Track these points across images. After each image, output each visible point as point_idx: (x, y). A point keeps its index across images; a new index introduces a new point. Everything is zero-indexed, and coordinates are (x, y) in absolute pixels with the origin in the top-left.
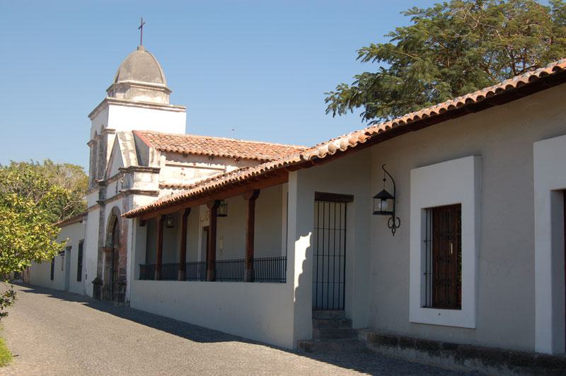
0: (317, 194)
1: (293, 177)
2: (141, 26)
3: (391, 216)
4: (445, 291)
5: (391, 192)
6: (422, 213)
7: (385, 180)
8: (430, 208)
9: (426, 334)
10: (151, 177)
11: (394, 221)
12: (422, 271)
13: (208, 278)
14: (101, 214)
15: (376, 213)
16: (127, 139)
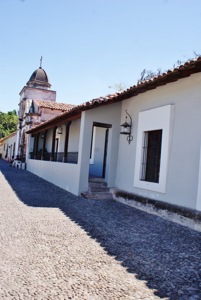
0: (94, 123)
1: (83, 114)
2: (41, 60)
3: (128, 135)
4: (151, 173)
5: (129, 122)
6: (143, 133)
7: (126, 117)
8: (147, 132)
9: (141, 194)
10: (38, 117)
11: (130, 137)
12: (141, 162)
13: (51, 160)
16: (30, 102)
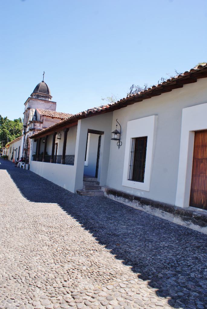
4: (138, 173)
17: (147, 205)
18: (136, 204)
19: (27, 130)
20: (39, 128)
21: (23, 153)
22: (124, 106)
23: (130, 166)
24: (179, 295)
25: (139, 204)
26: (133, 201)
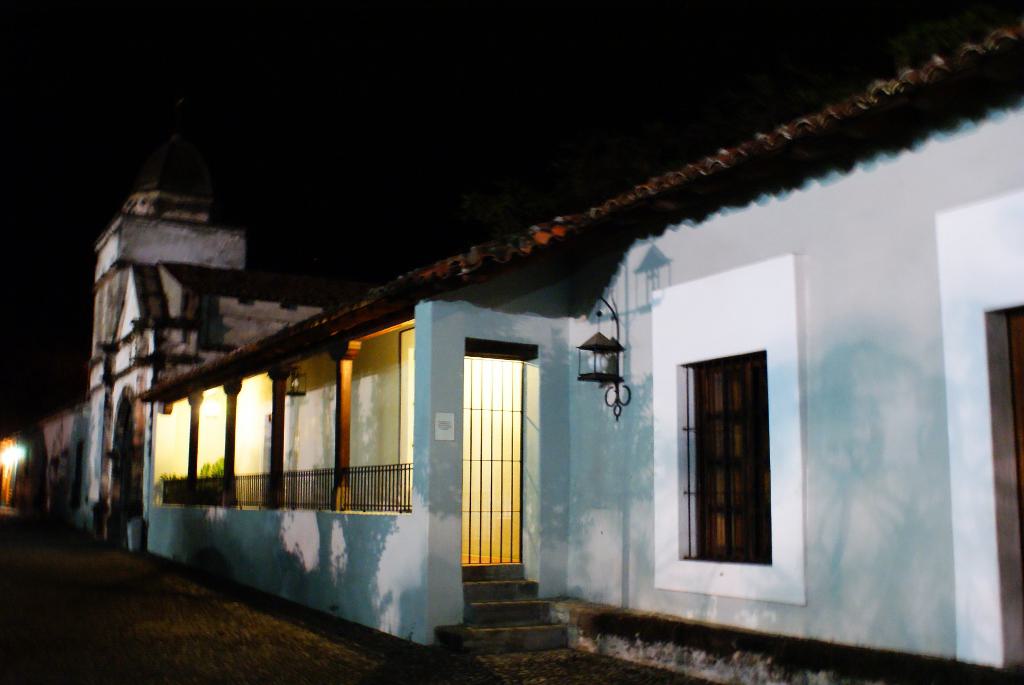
4: (732, 521)
12: (680, 489)
14: (108, 397)
15: (583, 377)
17: (816, 670)
18: (751, 672)
19: (122, 360)
20: (181, 349)
21: (104, 470)
22: (649, 448)
23: (687, 429)
24: (610, 651)
25: (770, 669)
26: (736, 655)
